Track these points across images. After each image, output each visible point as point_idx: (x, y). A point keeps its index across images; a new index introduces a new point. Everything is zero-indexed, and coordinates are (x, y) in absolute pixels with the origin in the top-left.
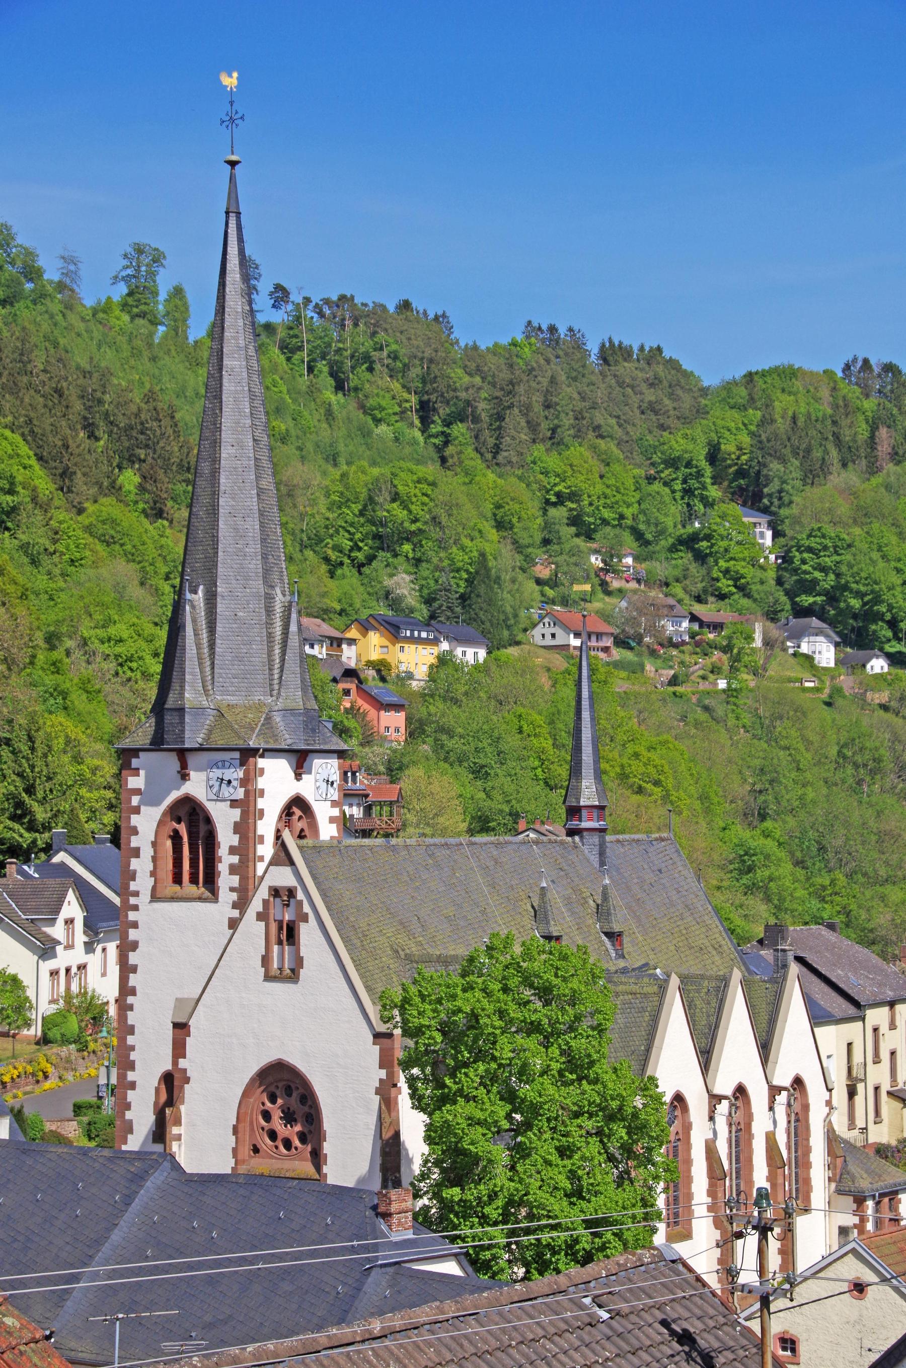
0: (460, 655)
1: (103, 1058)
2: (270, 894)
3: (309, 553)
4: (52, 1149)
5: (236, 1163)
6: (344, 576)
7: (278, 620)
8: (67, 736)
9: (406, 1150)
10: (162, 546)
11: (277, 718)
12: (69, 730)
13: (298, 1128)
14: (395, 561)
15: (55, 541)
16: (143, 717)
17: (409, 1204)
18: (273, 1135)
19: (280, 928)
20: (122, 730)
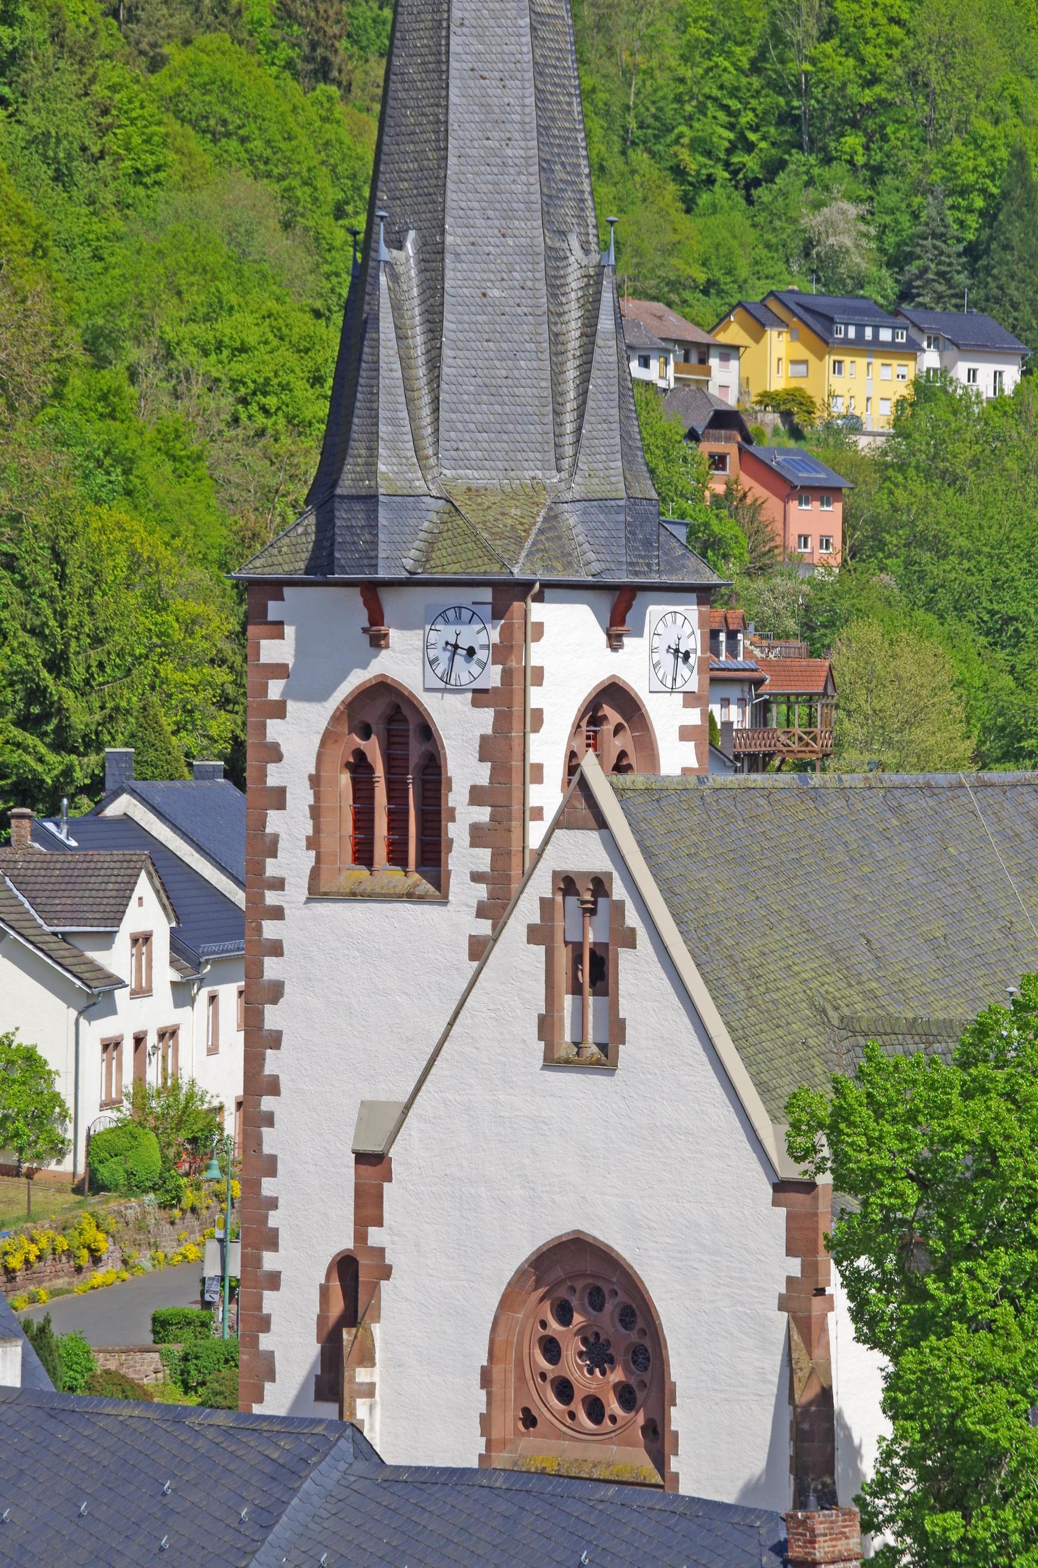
0: (963, 379)
1: (213, 1223)
2: (555, 889)
3: (639, 157)
4: (108, 1410)
5: (489, 1446)
6: (714, 208)
7: (574, 305)
8: (133, 553)
9: (846, 1429)
10: (327, 144)
11: (571, 517)
12: (136, 539)
13: (617, 1376)
14: (827, 173)
15: (103, 131)
16: (290, 512)
17: (854, 1542)
18: (564, 1390)
19: (577, 960)
20: (248, 539)
